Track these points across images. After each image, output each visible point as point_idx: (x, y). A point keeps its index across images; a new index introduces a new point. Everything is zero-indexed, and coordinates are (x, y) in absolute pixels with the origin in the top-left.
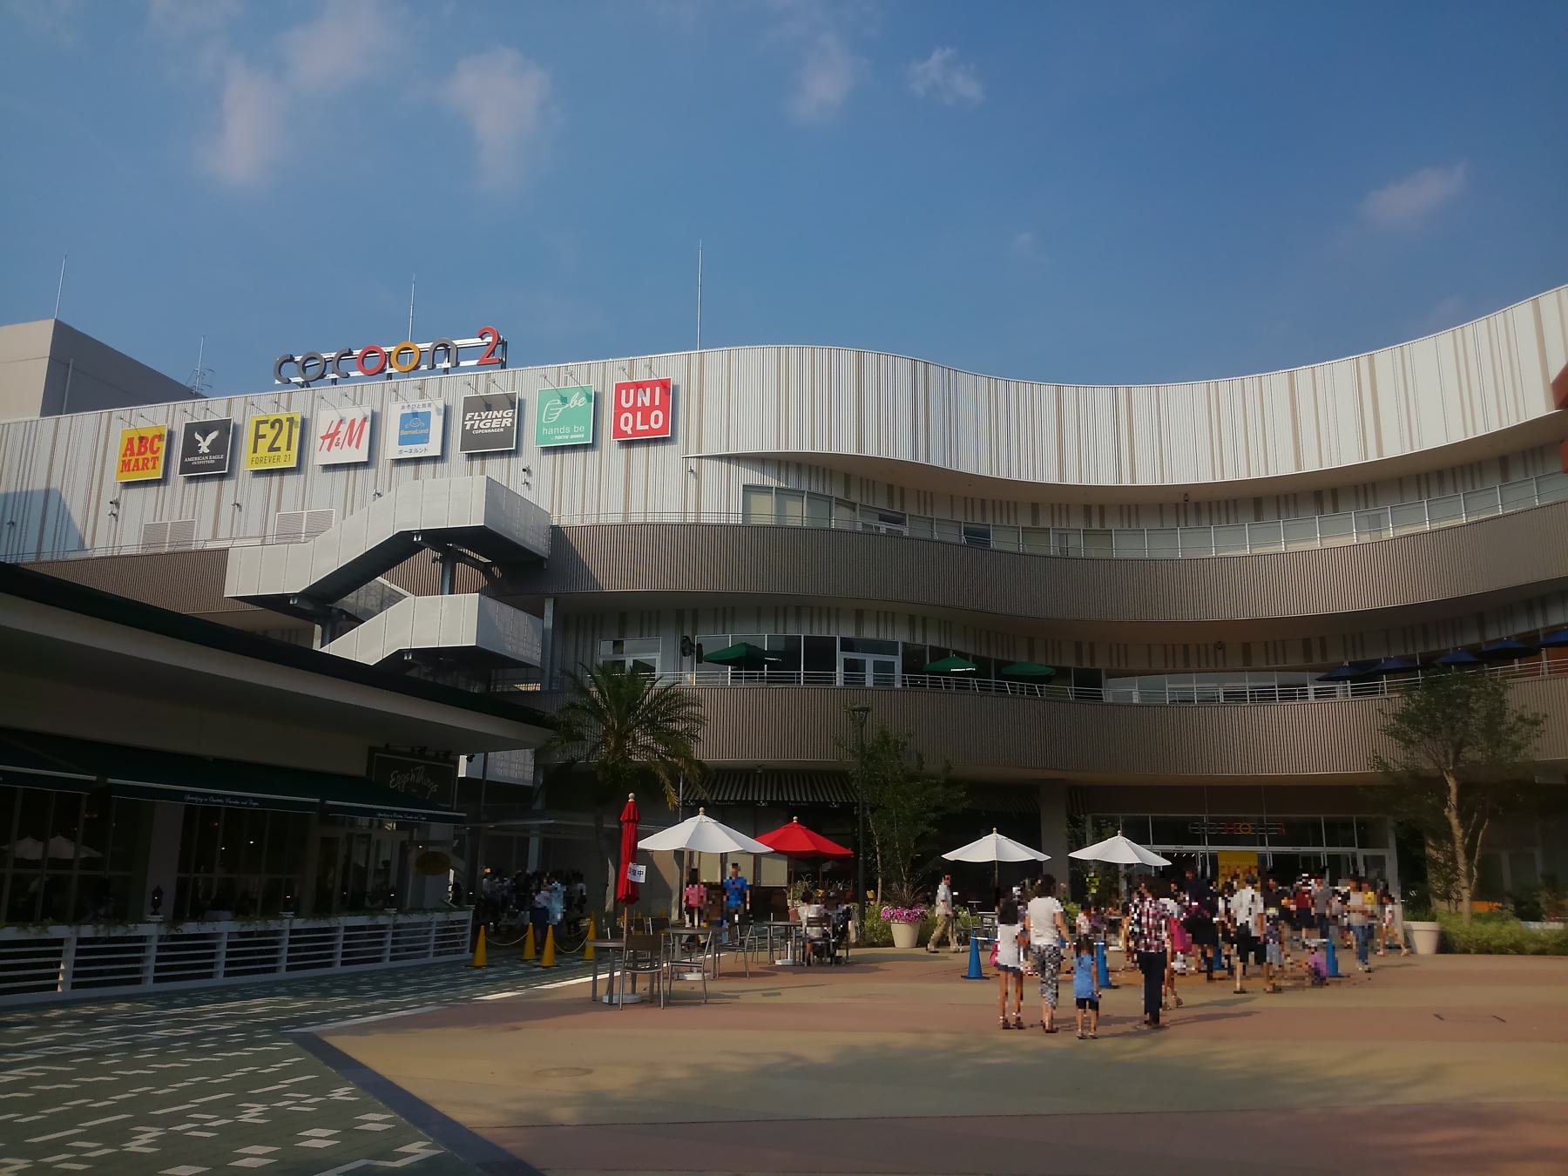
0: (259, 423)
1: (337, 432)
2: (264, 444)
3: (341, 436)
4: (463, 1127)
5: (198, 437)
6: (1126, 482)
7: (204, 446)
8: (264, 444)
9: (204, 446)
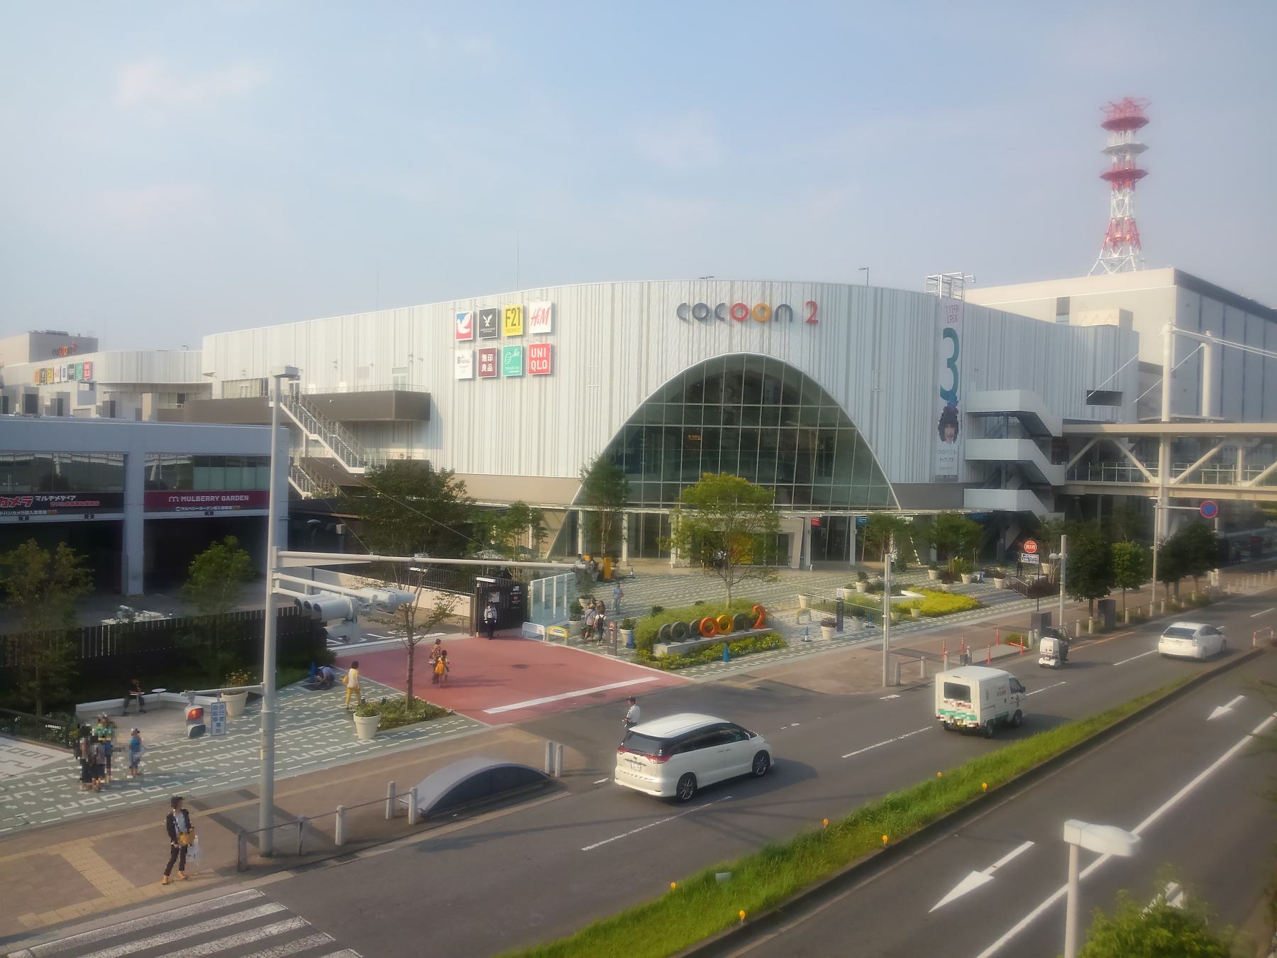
1: (538, 316)
2: (510, 321)
3: (539, 318)
5: (485, 318)
7: (487, 322)
8: (510, 321)
9: (487, 322)
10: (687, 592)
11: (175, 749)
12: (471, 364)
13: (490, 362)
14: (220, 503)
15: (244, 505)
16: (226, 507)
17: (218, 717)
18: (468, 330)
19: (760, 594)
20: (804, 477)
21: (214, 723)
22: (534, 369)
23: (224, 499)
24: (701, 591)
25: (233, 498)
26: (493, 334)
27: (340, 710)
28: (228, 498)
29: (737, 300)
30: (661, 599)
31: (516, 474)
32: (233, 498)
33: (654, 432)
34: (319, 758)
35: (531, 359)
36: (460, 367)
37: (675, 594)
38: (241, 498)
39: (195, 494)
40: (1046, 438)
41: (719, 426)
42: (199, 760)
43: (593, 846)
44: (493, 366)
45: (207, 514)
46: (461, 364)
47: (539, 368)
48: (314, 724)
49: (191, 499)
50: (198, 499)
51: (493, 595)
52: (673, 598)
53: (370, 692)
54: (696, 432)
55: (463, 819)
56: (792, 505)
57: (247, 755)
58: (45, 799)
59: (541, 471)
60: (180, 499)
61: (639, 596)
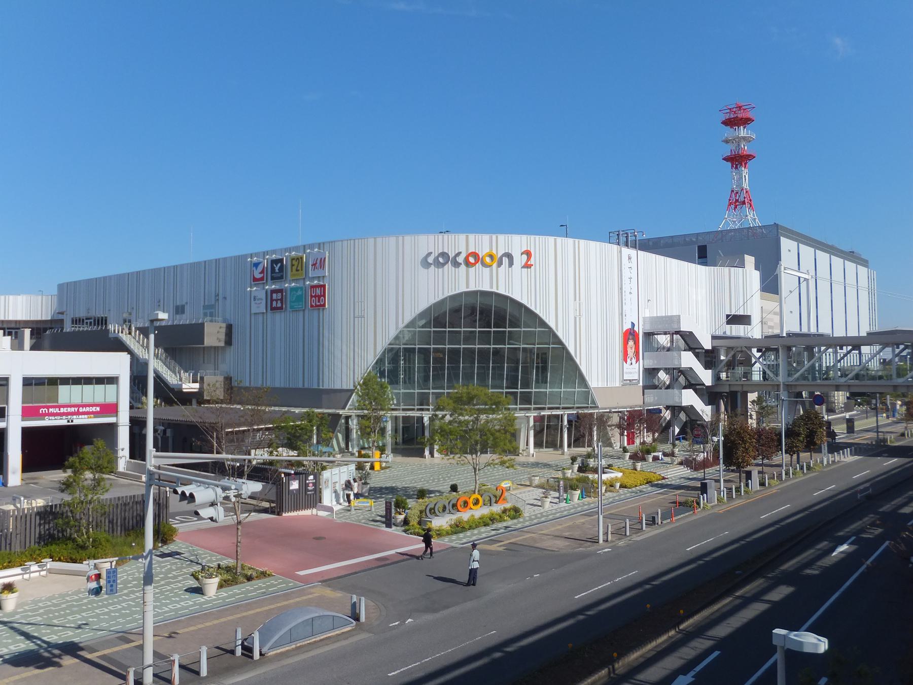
0: (610, 233)
1: (316, 263)
2: (294, 268)
3: (318, 265)
4: (626, 655)
5: (275, 266)
6: (577, 240)
7: (277, 269)
8: (294, 268)
9: (277, 269)
10: (440, 477)
11: (64, 606)
12: (264, 302)
13: (279, 300)
14: (78, 413)
15: (96, 414)
16: (83, 416)
17: (112, 579)
18: (262, 275)
19: (497, 477)
20: (526, 384)
21: (109, 585)
22: (314, 304)
23: (81, 410)
24: (451, 476)
25: (88, 409)
26: (281, 277)
27: (186, 574)
28: (84, 410)
29: (471, 250)
30: (420, 483)
31: (300, 386)
32: (88, 409)
33: (409, 352)
34: (177, 610)
35: (312, 296)
36: (256, 303)
37: (432, 478)
38: (93, 409)
39: (60, 407)
40: (700, 350)
41: (494, 346)
42: (84, 614)
43: (396, 672)
44: (282, 303)
45: (68, 421)
46: (256, 301)
47: (318, 304)
48: (168, 584)
49: (57, 410)
50: (62, 410)
51: (294, 483)
52: (430, 482)
53: (166, 568)
54: (442, 351)
55: (322, 646)
56: (519, 406)
57: (121, 609)
58: (5, 641)
59: (321, 384)
60: (48, 411)
61: (404, 481)
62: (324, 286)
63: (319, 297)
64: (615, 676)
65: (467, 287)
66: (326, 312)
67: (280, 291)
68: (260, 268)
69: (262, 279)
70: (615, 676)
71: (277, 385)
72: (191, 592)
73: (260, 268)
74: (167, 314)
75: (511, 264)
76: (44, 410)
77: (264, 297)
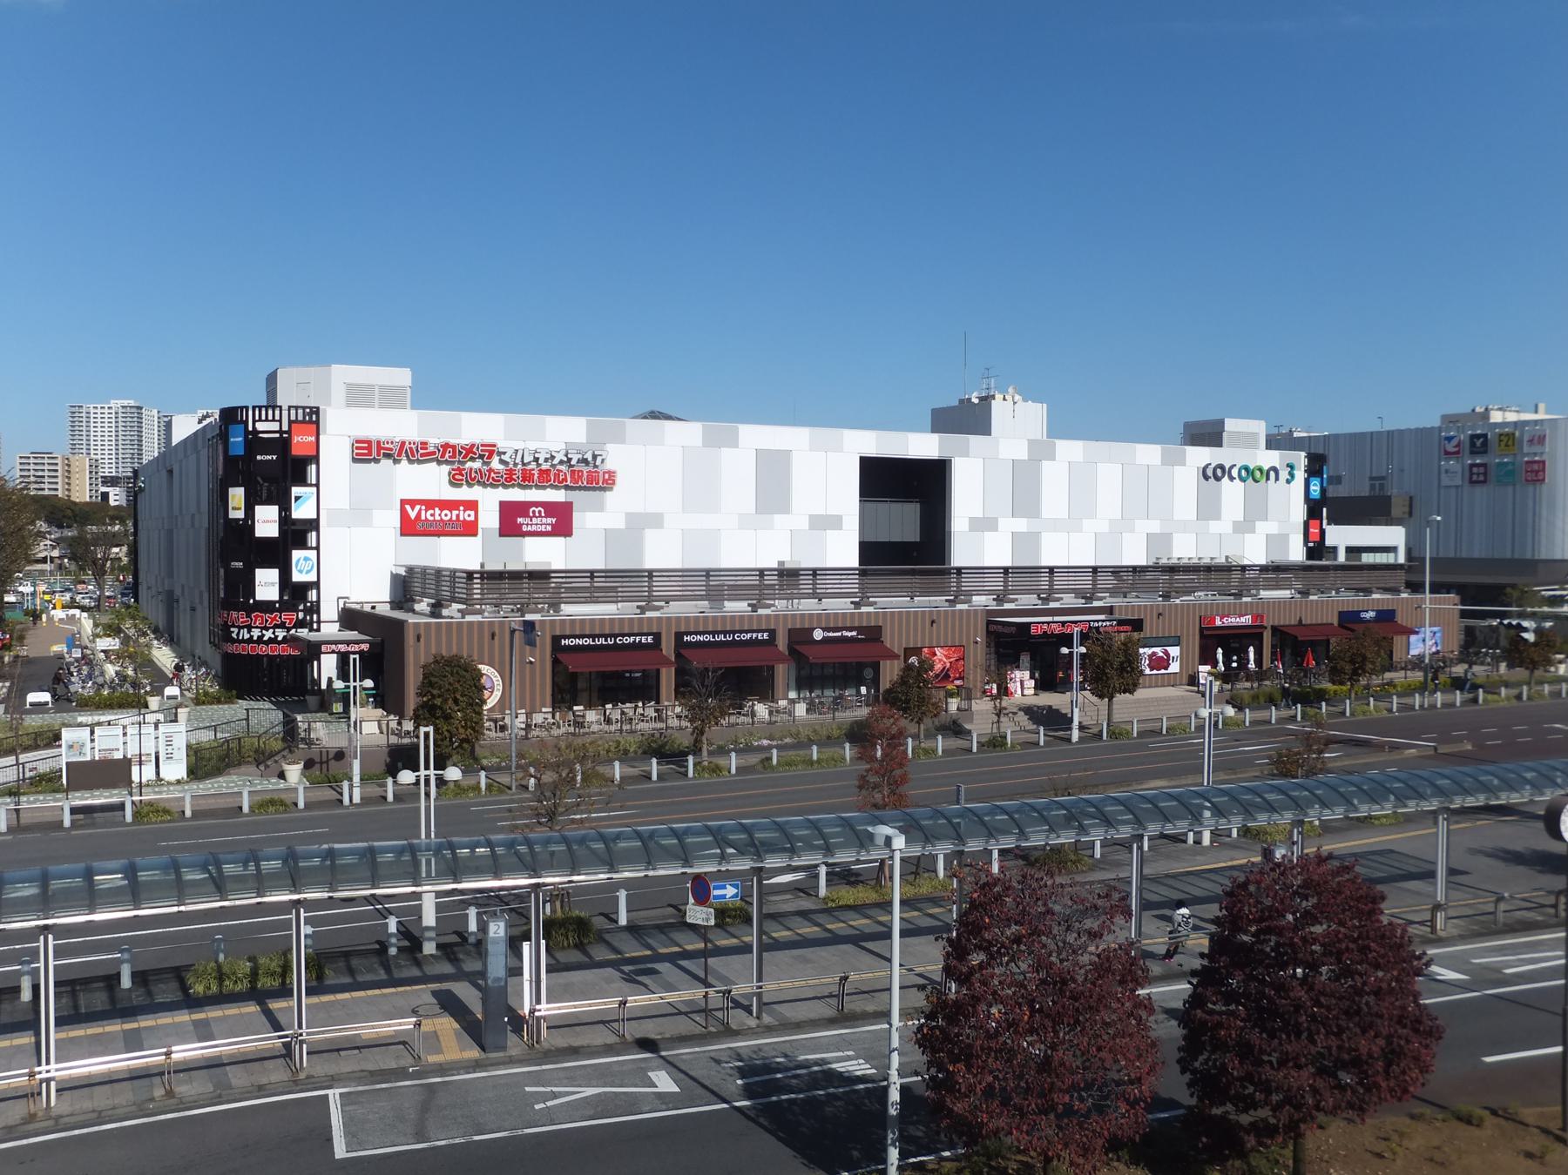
2: (1503, 444)
8: (1503, 444)
35: (1527, 472)
62: (1544, 462)
63: (1537, 472)
64: (771, 941)
65: (233, 508)
66: (1545, 487)
67: (1484, 465)
68: (1454, 442)
69: (1458, 453)
70: (771, 941)
71: (1476, 555)
72: (1505, 860)
73: (1454, 442)
74: (230, 517)
75: (1277, 479)
76: (537, 510)
77: (1460, 471)
